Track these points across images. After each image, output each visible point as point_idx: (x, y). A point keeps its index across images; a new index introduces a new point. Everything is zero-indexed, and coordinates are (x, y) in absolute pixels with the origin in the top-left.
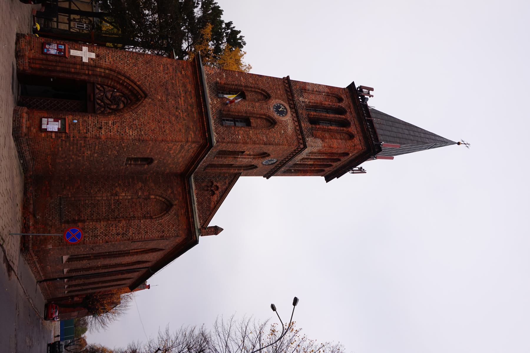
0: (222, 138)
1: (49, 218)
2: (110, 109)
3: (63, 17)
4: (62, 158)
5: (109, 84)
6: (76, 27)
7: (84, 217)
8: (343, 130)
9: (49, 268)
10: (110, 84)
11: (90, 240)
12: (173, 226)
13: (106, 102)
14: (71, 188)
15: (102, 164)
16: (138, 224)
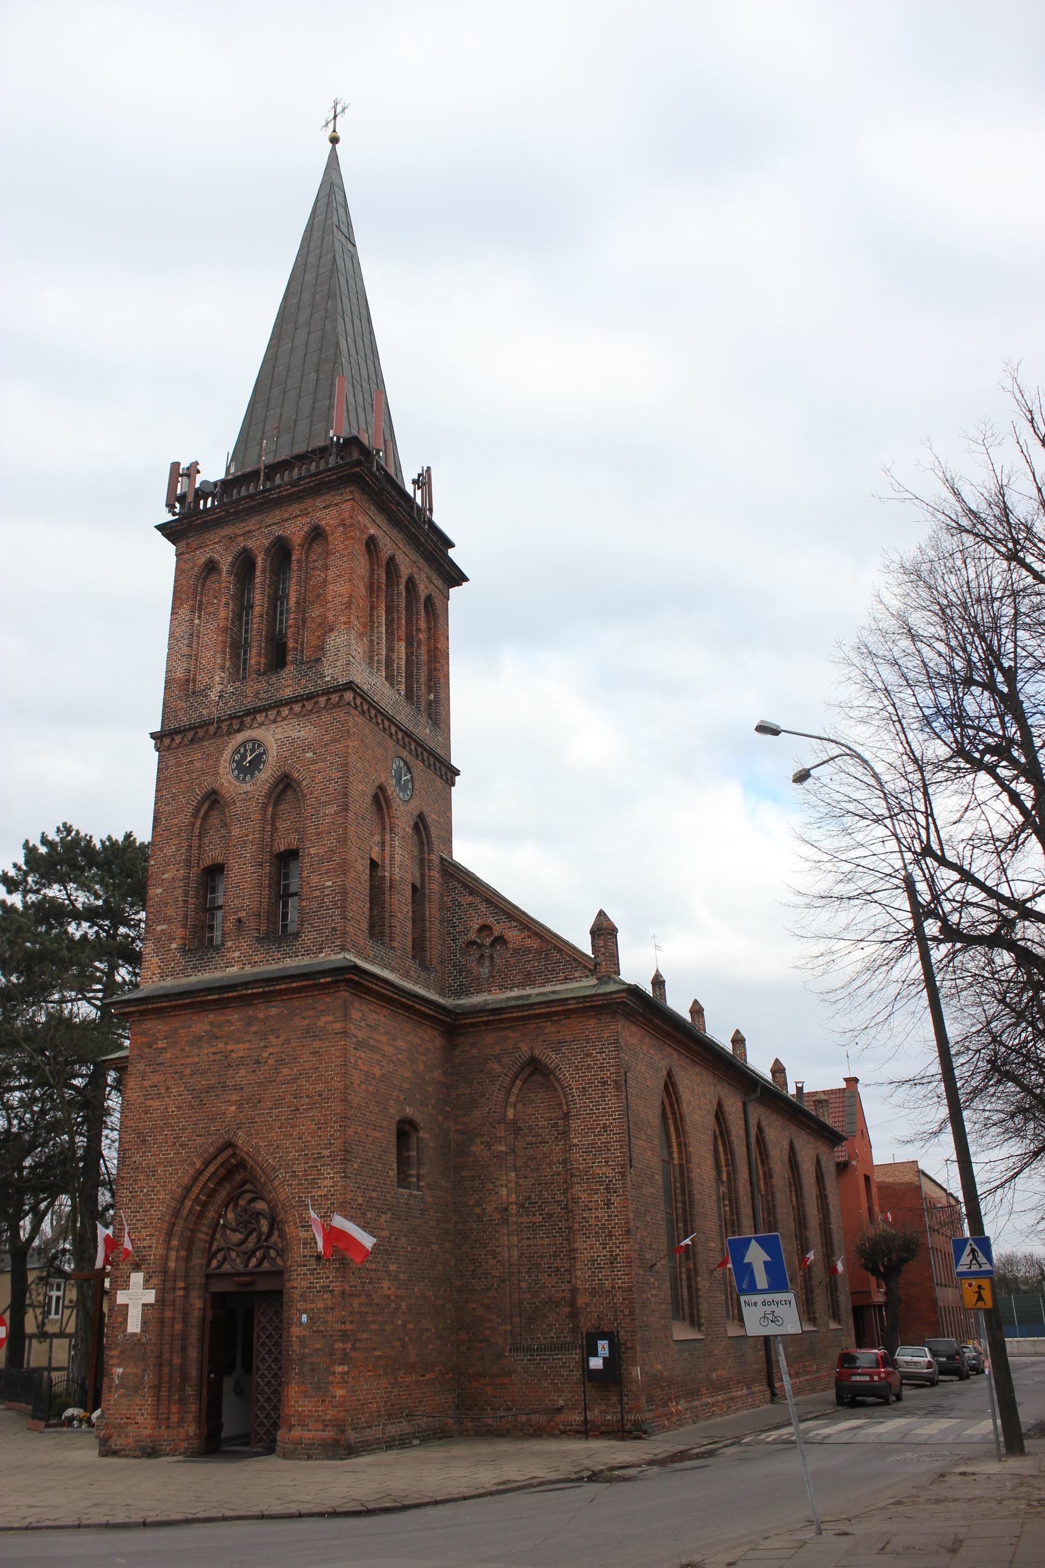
0: (333, 935)
1: (563, 1376)
2: (270, 1234)
3: (33, 1355)
4: (403, 1347)
5: (208, 1238)
6: (59, 1317)
7: (563, 1291)
8: (299, 561)
9: (719, 1373)
10: (207, 1234)
11: (622, 1275)
12: (589, 1055)
13: (252, 1245)
14: (487, 1325)
15: (419, 1249)
16: (583, 1152)
